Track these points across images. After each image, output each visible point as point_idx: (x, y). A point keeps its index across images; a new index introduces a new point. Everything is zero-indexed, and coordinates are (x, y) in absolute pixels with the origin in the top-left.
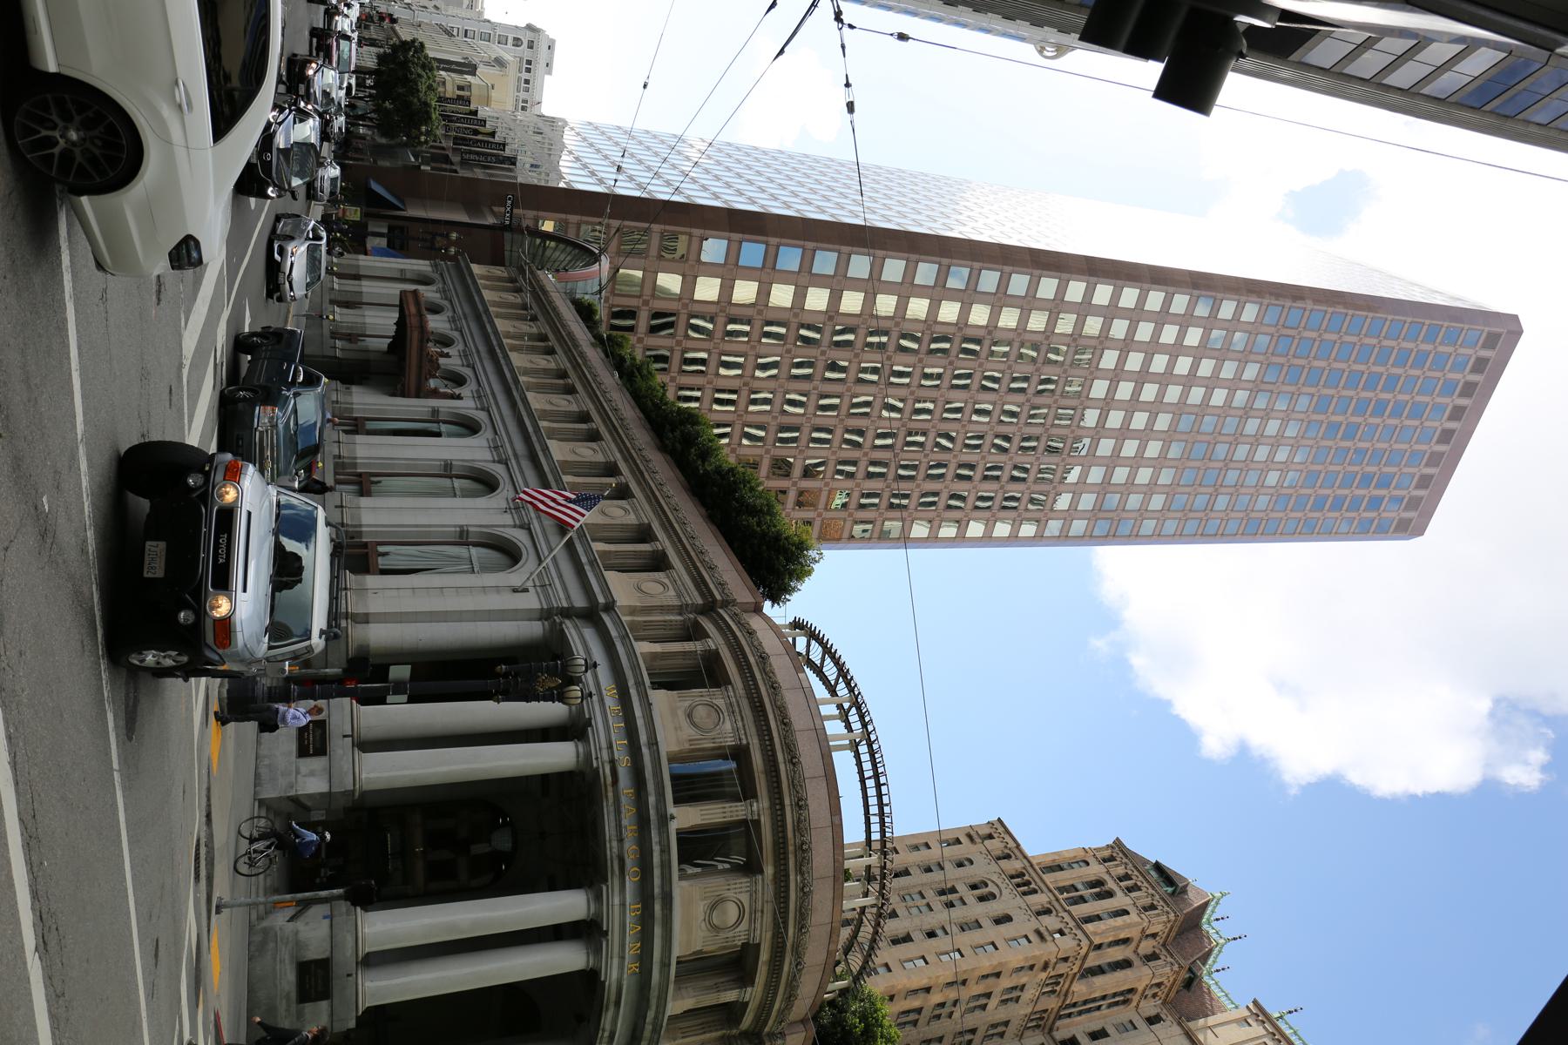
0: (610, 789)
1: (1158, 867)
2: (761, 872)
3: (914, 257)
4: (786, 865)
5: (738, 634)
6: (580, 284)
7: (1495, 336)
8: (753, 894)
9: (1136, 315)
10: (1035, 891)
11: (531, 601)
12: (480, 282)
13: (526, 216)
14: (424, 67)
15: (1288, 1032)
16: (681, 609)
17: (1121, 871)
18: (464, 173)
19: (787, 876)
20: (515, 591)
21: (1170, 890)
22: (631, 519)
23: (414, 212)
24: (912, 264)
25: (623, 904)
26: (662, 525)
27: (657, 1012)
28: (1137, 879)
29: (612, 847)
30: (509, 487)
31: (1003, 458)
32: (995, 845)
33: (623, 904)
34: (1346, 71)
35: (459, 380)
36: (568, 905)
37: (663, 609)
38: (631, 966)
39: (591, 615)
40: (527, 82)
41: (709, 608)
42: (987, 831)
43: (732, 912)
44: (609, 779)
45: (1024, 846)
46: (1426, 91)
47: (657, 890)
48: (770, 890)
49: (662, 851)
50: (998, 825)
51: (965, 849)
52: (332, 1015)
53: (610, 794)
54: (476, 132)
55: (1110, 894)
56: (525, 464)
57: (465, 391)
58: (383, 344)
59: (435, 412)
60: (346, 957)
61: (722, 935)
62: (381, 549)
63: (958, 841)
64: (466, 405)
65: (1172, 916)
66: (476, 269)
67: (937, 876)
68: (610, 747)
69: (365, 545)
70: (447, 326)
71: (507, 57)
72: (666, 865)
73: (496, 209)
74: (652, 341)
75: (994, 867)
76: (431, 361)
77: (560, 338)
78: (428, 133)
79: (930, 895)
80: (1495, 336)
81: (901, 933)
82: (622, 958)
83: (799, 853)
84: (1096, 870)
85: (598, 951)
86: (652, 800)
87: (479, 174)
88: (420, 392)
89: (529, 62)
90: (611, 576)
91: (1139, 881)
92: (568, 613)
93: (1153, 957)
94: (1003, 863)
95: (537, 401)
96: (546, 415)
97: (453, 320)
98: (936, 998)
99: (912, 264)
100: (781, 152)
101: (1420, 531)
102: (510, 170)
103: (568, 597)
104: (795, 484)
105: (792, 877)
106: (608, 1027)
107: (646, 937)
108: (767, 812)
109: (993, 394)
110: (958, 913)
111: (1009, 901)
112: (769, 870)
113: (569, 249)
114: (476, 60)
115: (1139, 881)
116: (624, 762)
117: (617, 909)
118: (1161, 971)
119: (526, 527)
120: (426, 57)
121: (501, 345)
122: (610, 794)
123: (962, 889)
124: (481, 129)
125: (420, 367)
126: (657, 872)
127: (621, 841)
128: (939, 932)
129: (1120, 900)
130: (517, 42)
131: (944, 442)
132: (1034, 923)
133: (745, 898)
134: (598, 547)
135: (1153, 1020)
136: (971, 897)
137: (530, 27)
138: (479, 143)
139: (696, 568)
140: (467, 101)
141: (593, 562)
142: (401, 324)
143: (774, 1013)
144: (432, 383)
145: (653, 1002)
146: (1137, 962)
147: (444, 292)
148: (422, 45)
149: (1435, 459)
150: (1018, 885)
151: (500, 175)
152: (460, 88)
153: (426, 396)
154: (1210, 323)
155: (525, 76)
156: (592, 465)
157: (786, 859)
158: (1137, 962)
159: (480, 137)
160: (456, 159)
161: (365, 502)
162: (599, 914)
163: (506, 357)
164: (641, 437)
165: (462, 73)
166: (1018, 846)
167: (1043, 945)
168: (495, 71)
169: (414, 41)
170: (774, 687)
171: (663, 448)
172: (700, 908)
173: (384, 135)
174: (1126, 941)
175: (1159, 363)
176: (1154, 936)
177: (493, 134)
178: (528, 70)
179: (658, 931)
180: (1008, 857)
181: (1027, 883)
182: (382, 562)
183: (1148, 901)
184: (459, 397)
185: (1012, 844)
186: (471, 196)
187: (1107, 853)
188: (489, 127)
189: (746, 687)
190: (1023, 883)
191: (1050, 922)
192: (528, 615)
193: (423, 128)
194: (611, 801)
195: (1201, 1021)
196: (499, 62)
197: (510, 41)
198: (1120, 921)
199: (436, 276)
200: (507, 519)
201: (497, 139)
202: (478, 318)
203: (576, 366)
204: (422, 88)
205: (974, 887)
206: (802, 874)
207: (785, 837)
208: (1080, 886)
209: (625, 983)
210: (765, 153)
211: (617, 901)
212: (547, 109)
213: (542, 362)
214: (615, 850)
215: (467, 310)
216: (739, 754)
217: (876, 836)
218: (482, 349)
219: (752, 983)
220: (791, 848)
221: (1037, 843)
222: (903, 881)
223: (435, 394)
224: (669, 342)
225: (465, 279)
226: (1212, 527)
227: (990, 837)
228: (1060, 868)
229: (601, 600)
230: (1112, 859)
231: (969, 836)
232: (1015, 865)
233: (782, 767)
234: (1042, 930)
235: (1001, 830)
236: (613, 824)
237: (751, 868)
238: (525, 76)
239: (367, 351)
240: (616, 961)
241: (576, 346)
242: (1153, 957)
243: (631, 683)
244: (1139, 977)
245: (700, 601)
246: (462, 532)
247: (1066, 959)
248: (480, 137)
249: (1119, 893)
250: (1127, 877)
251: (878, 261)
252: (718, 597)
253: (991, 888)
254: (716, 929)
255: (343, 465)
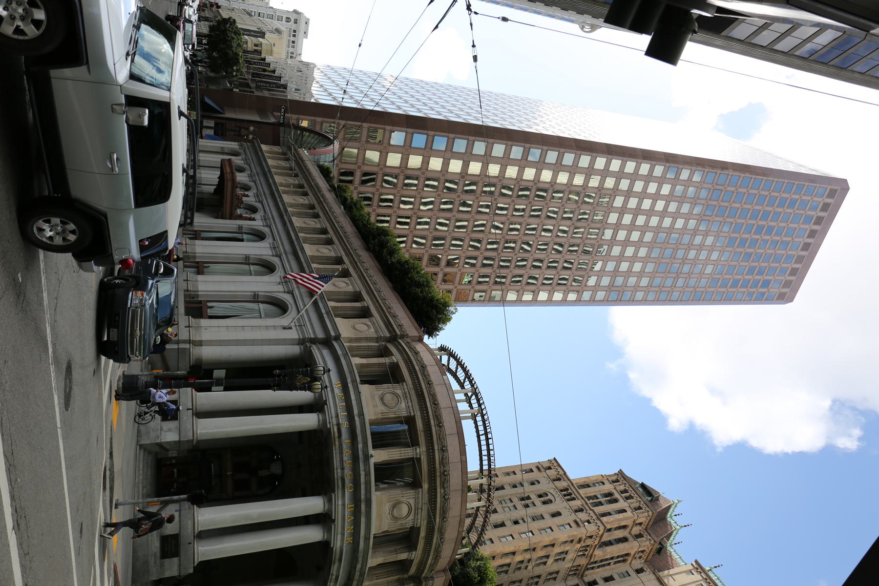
0: (337, 440)
1: (643, 486)
2: (421, 487)
3: (510, 143)
4: (435, 483)
5: (409, 353)
6: (322, 156)
7: (831, 192)
8: (416, 499)
9: (634, 177)
10: (574, 499)
11: (293, 334)
12: (266, 154)
13: (292, 118)
14: (235, 33)
15: (714, 578)
16: (377, 340)
17: (622, 488)
18: (257, 93)
19: (436, 489)
20: (285, 328)
21: (650, 498)
22: (350, 289)
23: (229, 115)
24: (509, 147)
25: (344, 505)
26: (367, 292)
27: (362, 565)
28: (631, 492)
29: (338, 473)
30: (281, 270)
31: (558, 256)
32: (552, 473)
33: (344, 505)
34: (775, 48)
35: (254, 210)
36: (313, 504)
37: (367, 339)
38: (348, 539)
39: (327, 342)
40: (293, 42)
41: (393, 339)
42: (548, 465)
43: (405, 509)
44: (336, 435)
45: (568, 473)
46: (797, 53)
47: (363, 497)
48: (426, 496)
49: (366, 475)
50: (554, 462)
51: (535, 475)
52: (180, 566)
53: (337, 443)
54: (265, 70)
55: (616, 501)
56: (291, 257)
57: (257, 216)
58: (212, 189)
59: (240, 227)
60: (188, 533)
61: (399, 522)
62: (209, 304)
63: (531, 471)
64: (258, 224)
65: (650, 513)
66: (264, 147)
67: (519, 490)
68: (337, 416)
69: (200, 302)
70: (247, 179)
71: (282, 28)
72: (368, 483)
73: (275, 114)
74: (363, 189)
75: (551, 485)
76: (238, 199)
77: (311, 186)
78: (237, 71)
79: (516, 500)
80: (831, 192)
81: (499, 521)
82: (343, 534)
83: (443, 477)
84: (608, 487)
85: (329, 530)
86: (360, 446)
87: (266, 94)
88: (232, 216)
89: (295, 31)
90: (338, 321)
91: (632, 493)
92: (314, 341)
93: (640, 536)
94: (556, 483)
95: (297, 222)
96: (302, 230)
97: (250, 176)
98: (518, 558)
99: (509, 147)
100: (436, 83)
101: (791, 299)
102: (284, 92)
103: (314, 332)
104: (442, 270)
105: (438, 490)
106: (335, 573)
107: (356, 523)
108: (425, 454)
109: (549, 218)
110: (531, 511)
111: (559, 504)
112: (426, 486)
113: (316, 136)
114: (264, 30)
115: (632, 493)
116: (345, 425)
117: (340, 507)
118: (644, 544)
119: (291, 292)
120: (237, 28)
121: (278, 191)
122: (337, 443)
123: (534, 497)
124: (267, 69)
125: (232, 202)
126: (363, 487)
127: (343, 469)
128: (521, 521)
129: (622, 504)
130: (288, 20)
131: (526, 247)
132: (573, 517)
133: (412, 501)
134: (331, 304)
135: (639, 571)
136: (538, 501)
137: (295, 12)
138: (266, 77)
139: (386, 317)
140: (260, 53)
141: (328, 313)
142: (221, 178)
143: (428, 566)
144: (239, 211)
145: (360, 559)
146: (630, 539)
147: (246, 160)
148: (234, 20)
149: (800, 260)
150: (565, 495)
151: (278, 95)
152: (256, 45)
153: (235, 219)
154: (675, 182)
155: (292, 39)
156: (328, 258)
157: (435, 480)
158: (630, 539)
159: (266, 73)
160: (253, 85)
161: (200, 278)
162: (330, 510)
163: (281, 197)
164: (356, 243)
165: (257, 37)
166: (565, 473)
167: (578, 529)
168: (276, 36)
169: (230, 18)
170: (429, 383)
171: (368, 249)
172: (387, 507)
173: (212, 71)
174: (625, 527)
175: (647, 204)
176: (640, 524)
177: (274, 71)
178: (294, 36)
179: (363, 520)
180: (559, 479)
181: (570, 494)
182: (210, 312)
183: (637, 505)
184: (254, 219)
185: (561, 472)
186: (262, 106)
187: (614, 478)
188: (272, 68)
189: (414, 383)
190: (568, 494)
191: (582, 516)
192: (291, 342)
193: (235, 68)
194: (337, 447)
195: (666, 572)
196: (278, 31)
197: (284, 19)
198: (621, 516)
199: (241, 151)
200: (280, 288)
201: (276, 74)
202: (265, 175)
203: (320, 202)
204: (235, 45)
205: (540, 496)
206: (444, 488)
207: (435, 468)
208: (599, 496)
209: (344, 548)
210: (427, 83)
211: (340, 503)
212: (305, 58)
213: (291, 180)
214: (339, 474)
215: (259, 171)
216: (410, 421)
217: (485, 467)
218: (267, 192)
219: (416, 549)
220: (438, 474)
221: (576, 472)
222: (500, 492)
223: (240, 217)
224: (372, 190)
225: (258, 152)
226: (676, 295)
227: (550, 468)
228: (588, 486)
229: (333, 334)
230: (617, 481)
231: (538, 468)
232: (563, 484)
233: (433, 428)
234: (578, 520)
235: (555, 464)
236: (338, 460)
237: (415, 484)
238: (292, 39)
239: (202, 193)
240: (339, 537)
241: (320, 191)
242: (640, 536)
243: (349, 380)
244: (633, 547)
245: (388, 335)
246: (255, 295)
247: (591, 537)
248: (266, 73)
249: (621, 500)
250: (625, 491)
251: (544, 152)
252: (398, 333)
253: (550, 497)
254: (395, 519)
255: (188, 257)
